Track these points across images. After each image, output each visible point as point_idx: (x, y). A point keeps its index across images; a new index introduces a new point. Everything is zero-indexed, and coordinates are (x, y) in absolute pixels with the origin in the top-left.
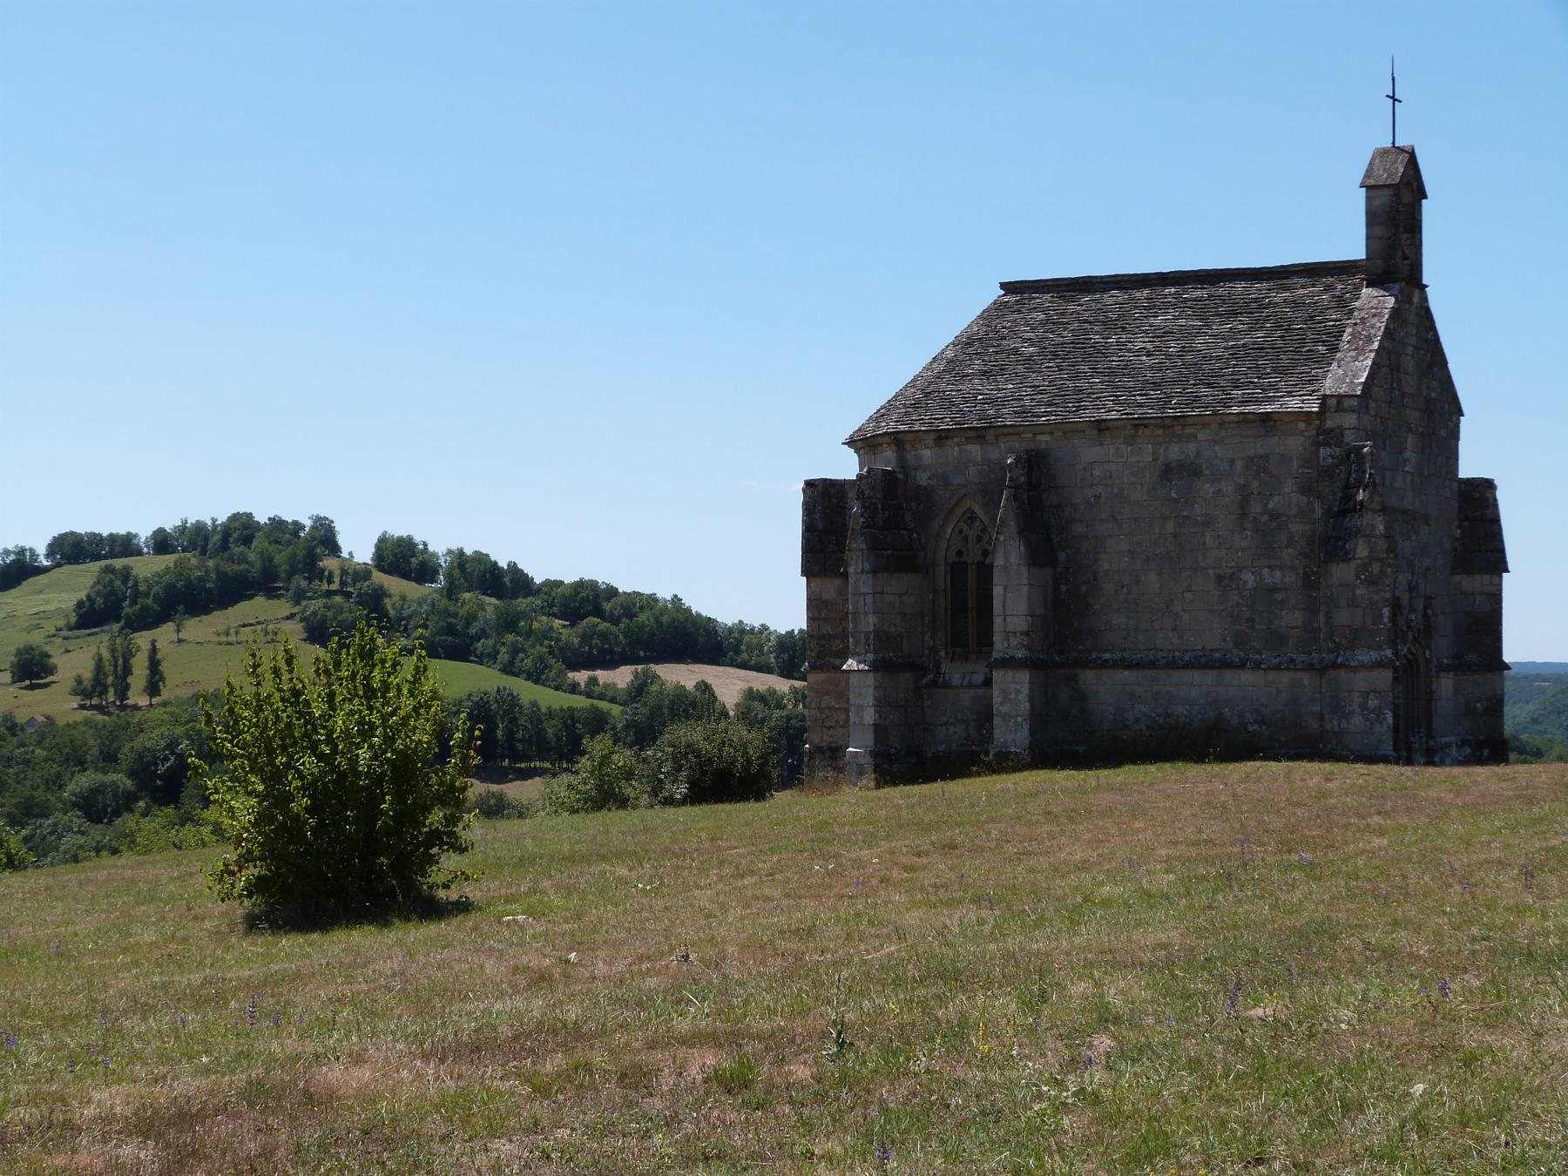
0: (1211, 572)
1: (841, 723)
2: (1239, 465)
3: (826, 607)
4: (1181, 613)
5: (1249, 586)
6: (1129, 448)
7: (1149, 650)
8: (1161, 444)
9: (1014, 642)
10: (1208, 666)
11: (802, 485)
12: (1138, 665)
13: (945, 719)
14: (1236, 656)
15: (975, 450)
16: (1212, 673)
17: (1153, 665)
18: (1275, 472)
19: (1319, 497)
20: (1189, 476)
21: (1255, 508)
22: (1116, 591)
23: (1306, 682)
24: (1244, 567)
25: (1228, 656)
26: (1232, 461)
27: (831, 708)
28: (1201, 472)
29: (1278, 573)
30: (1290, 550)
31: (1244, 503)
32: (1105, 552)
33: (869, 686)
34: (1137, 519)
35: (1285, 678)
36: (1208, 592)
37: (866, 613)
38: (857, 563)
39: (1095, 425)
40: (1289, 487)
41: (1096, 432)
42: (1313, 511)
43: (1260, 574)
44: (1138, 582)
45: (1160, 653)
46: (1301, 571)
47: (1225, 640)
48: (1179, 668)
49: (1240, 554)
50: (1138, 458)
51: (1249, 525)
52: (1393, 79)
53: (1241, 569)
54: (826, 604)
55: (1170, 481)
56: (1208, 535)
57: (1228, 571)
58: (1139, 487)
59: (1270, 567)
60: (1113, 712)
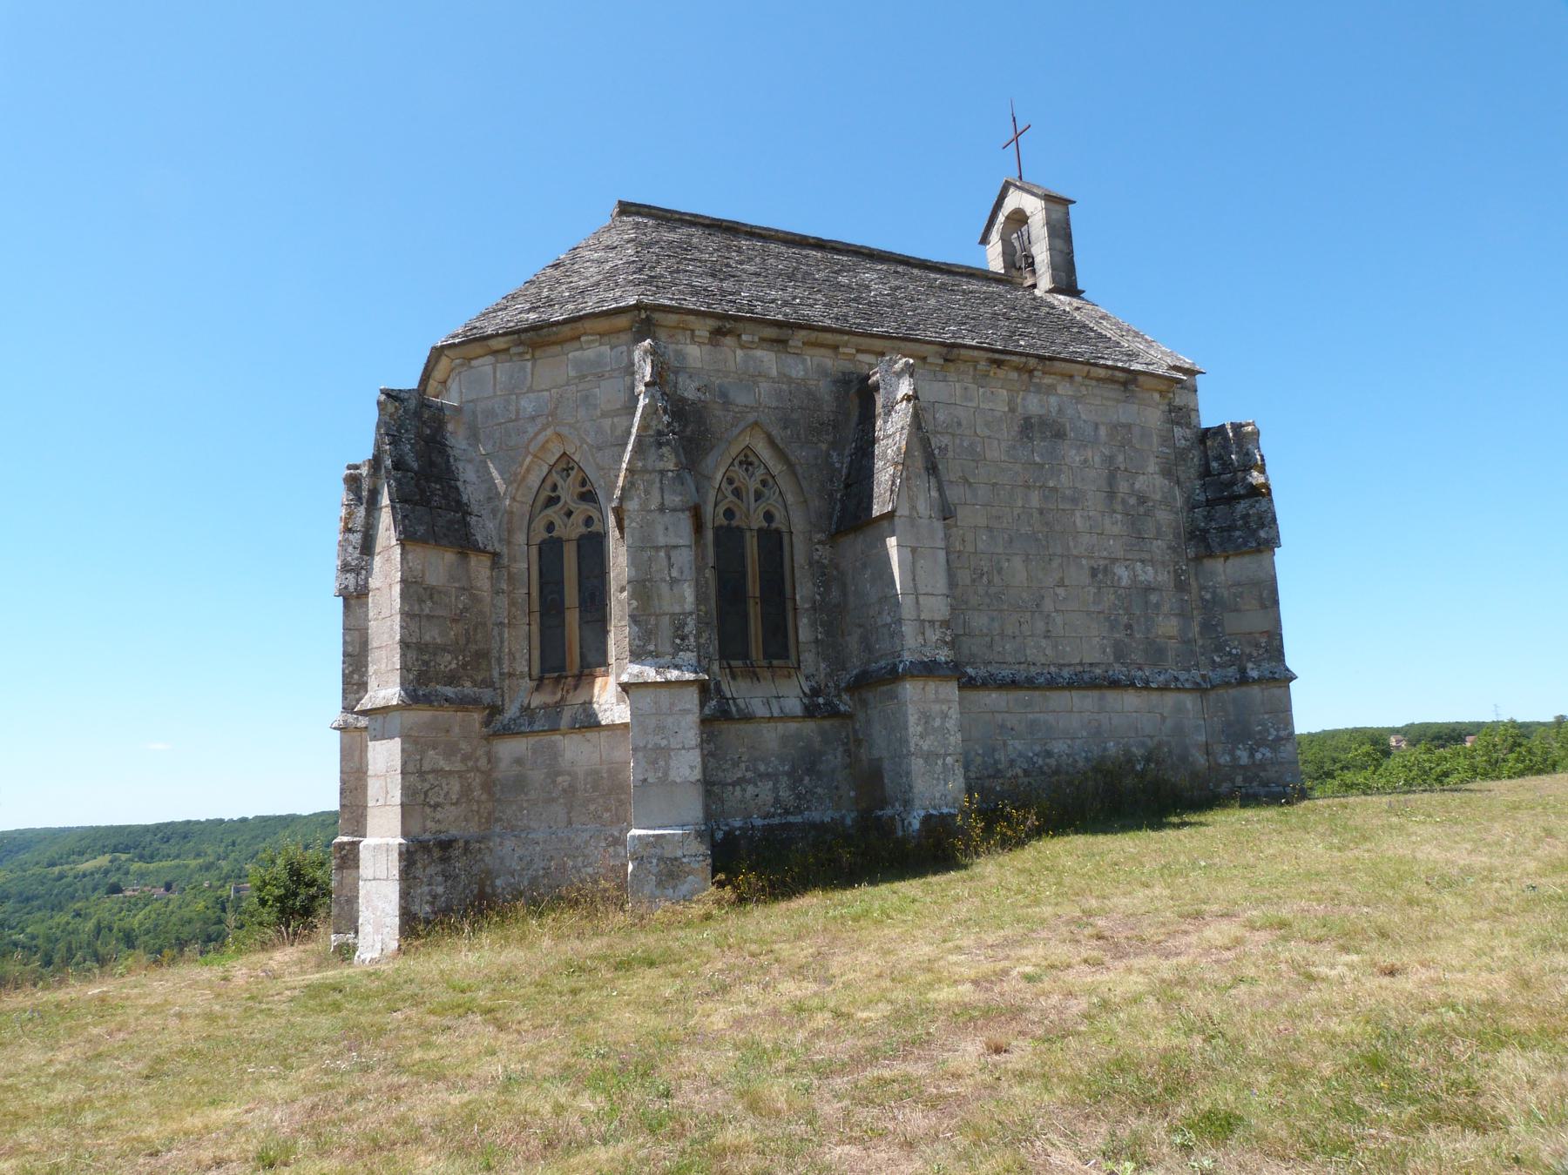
0: (1084, 562)
1: (454, 797)
2: (1103, 431)
3: (431, 597)
5: (1124, 583)
6: (981, 390)
7: (1020, 663)
9: (933, 636)
10: (1093, 685)
11: (377, 395)
12: (1013, 684)
13: (740, 775)
14: (1118, 671)
15: (767, 359)
17: (1030, 684)
18: (1138, 446)
19: (1178, 483)
21: (1123, 487)
22: (974, 581)
23: (1189, 705)
25: (1111, 673)
26: (1096, 426)
28: (1065, 435)
31: (1111, 479)
32: (957, 526)
33: (687, 711)
34: (994, 485)
35: (1170, 699)
37: (674, 582)
39: (944, 350)
40: (1152, 467)
42: (1175, 498)
44: (1000, 571)
45: (1032, 669)
46: (1172, 569)
49: (1111, 542)
50: (991, 406)
51: (1119, 508)
53: (1114, 560)
54: (432, 592)
55: (1031, 439)
56: (1078, 514)
57: (1102, 562)
59: (1142, 561)
60: (980, 752)
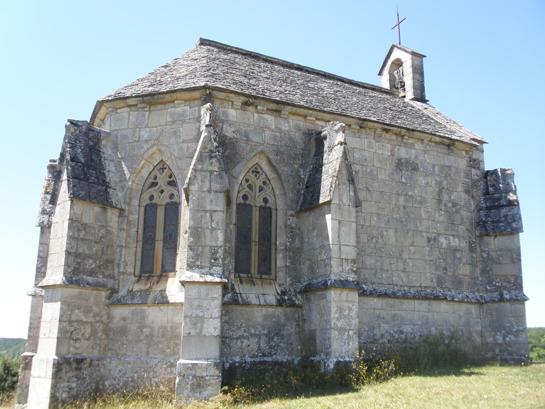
0: (424, 234)
2: (437, 169)
3: (85, 229)
4: (408, 260)
6: (377, 144)
7: (389, 284)
8: (396, 146)
9: (347, 267)
12: (385, 295)
13: (240, 334)
14: (439, 291)
16: (426, 302)
17: (394, 295)
20: (412, 170)
21: (445, 197)
22: (368, 240)
23: (473, 311)
24: (441, 234)
25: (435, 292)
26: (434, 166)
27: (78, 321)
28: (418, 169)
29: (457, 240)
30: (462, 226)
31: (440, 193)
33: (213, 298)
34: (382, 192)
35: (464, 307)
36: (423, 247)
37: (213, 229)
38: (202, 181)
40: (460, 189)
41: (358, 128)
42: (471, 205)
43: (449, 240)
44: (382, 236)
45: (396, 287)
46: (468, 240)
47: (432, 281)
48: (408, 298)
49: (438, 225)
51: (443, 208)
52: (398, 15)
53: (439, 234)
54: (85, 226)
55: (401, 170)
56: (422, 209)
57: (433, 235)
58: (383, 171)
59: (453, 236)
60: (367, 329)
